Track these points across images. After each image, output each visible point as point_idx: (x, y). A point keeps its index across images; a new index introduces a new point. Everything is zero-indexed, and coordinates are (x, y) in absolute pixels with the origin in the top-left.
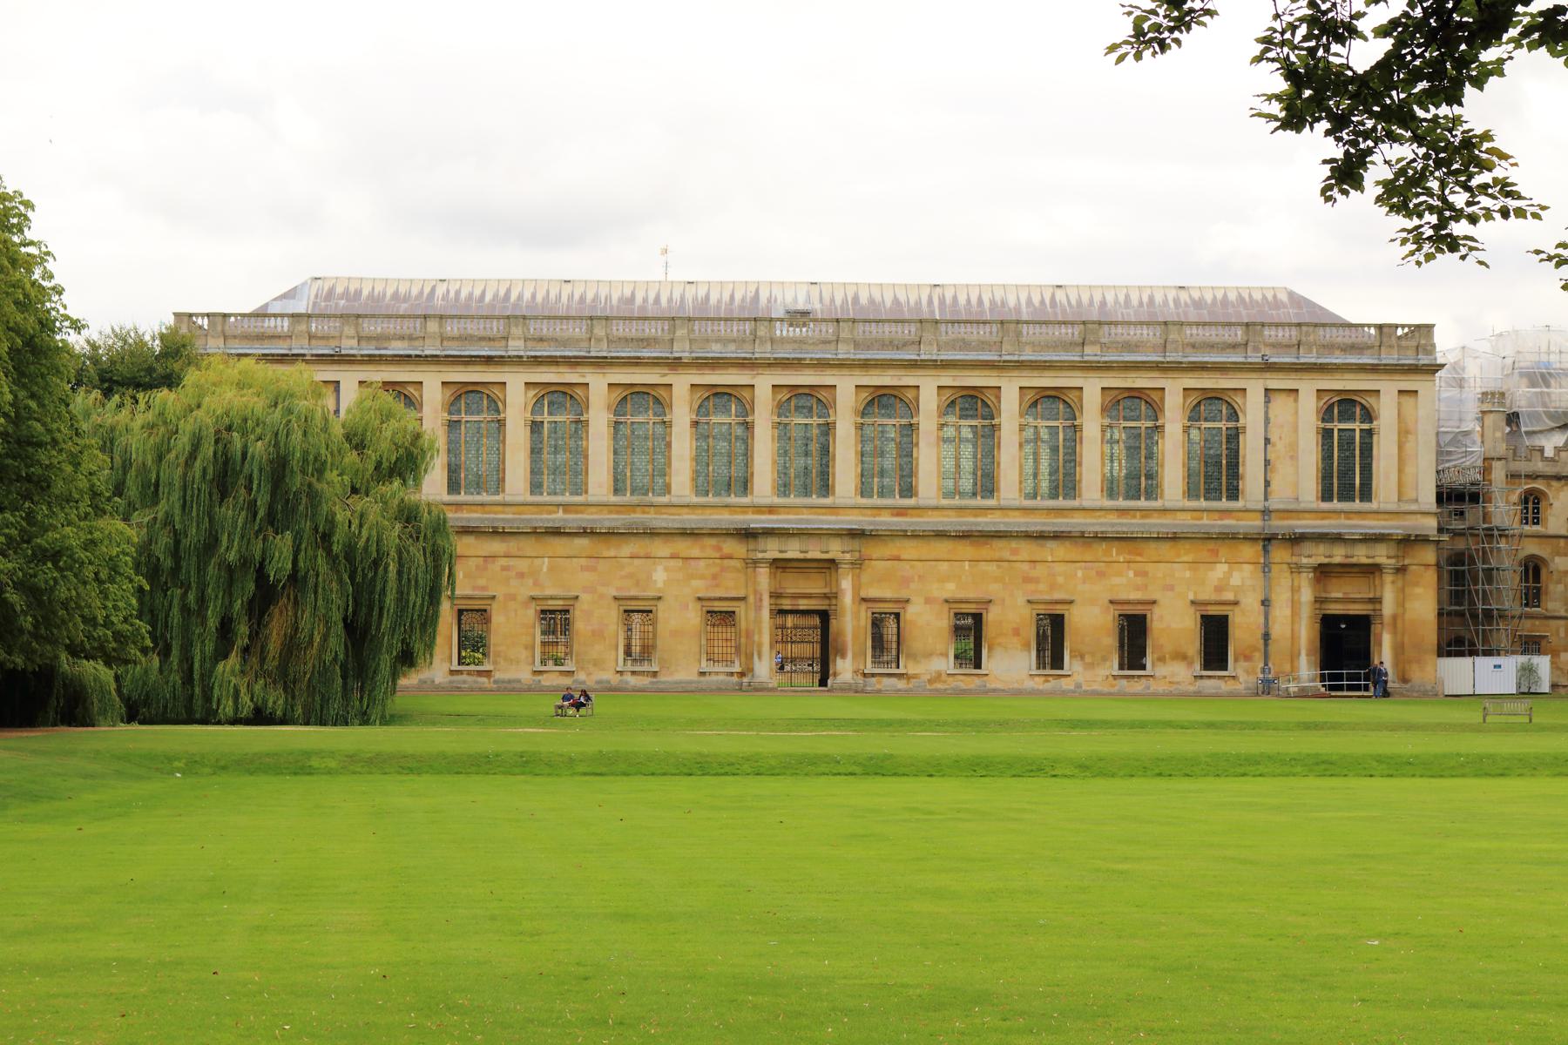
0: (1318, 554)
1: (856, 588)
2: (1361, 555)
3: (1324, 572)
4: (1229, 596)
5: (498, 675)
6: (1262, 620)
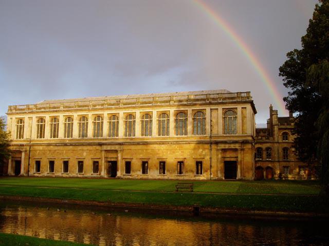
0: (222, 146)
1: (122, 156)
2: (232, 146)
3: (224, 150)
4: (202, 157)
5: (56, 174)
6: (210, 162)
